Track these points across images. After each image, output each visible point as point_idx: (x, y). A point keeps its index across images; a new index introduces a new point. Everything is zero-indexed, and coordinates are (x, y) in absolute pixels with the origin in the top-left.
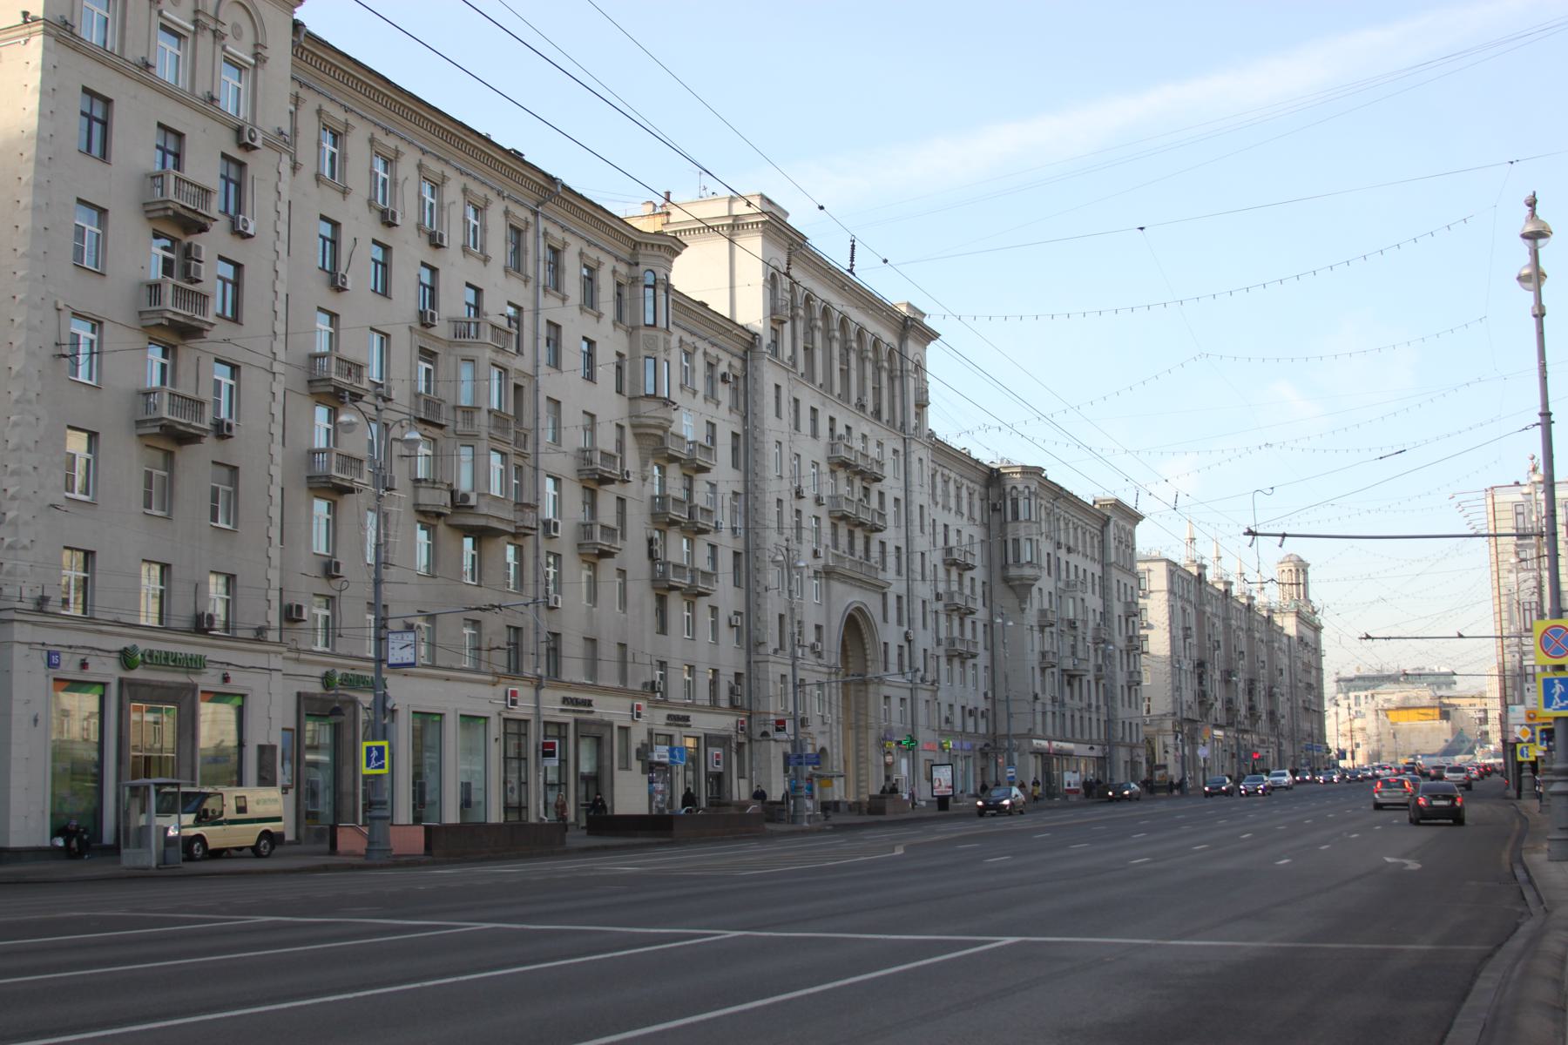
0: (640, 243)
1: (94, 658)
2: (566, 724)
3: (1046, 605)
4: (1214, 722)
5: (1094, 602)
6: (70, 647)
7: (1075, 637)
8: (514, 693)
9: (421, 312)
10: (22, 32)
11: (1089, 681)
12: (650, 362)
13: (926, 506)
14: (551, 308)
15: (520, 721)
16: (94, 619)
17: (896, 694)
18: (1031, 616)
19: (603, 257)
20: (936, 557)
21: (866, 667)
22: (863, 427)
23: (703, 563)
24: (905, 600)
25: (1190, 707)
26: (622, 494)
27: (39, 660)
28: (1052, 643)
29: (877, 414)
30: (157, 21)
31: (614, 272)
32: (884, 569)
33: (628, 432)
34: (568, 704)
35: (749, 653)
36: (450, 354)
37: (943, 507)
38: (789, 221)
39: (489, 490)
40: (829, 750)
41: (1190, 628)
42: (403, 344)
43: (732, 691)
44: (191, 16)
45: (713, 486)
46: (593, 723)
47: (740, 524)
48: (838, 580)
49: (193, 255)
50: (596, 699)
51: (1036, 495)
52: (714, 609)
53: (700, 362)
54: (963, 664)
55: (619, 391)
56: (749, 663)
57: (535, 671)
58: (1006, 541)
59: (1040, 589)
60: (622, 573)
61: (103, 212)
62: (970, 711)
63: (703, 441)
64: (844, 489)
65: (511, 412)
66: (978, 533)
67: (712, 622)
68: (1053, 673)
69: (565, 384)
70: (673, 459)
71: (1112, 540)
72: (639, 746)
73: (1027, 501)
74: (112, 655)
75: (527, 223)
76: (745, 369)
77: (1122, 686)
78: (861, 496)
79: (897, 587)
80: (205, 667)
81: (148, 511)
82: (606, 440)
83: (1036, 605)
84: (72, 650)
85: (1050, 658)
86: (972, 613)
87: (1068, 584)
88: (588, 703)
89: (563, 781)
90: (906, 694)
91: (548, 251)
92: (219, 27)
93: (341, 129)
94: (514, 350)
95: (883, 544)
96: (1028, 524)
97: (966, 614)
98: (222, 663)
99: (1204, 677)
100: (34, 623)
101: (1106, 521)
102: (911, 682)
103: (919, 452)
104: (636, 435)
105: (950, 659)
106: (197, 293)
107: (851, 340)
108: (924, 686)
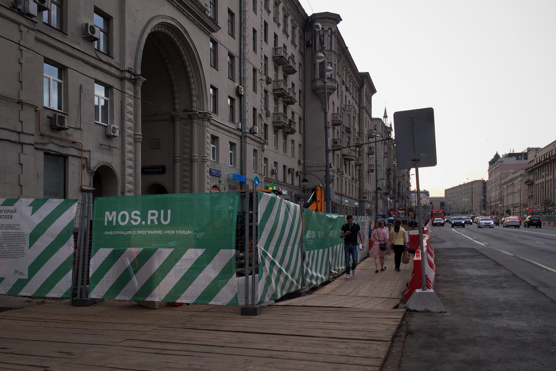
7: (349, 138)
21: (192, 102)
40: (117, 170)
62: (289, 170)
73: (329, 38)
96: (330, 53)
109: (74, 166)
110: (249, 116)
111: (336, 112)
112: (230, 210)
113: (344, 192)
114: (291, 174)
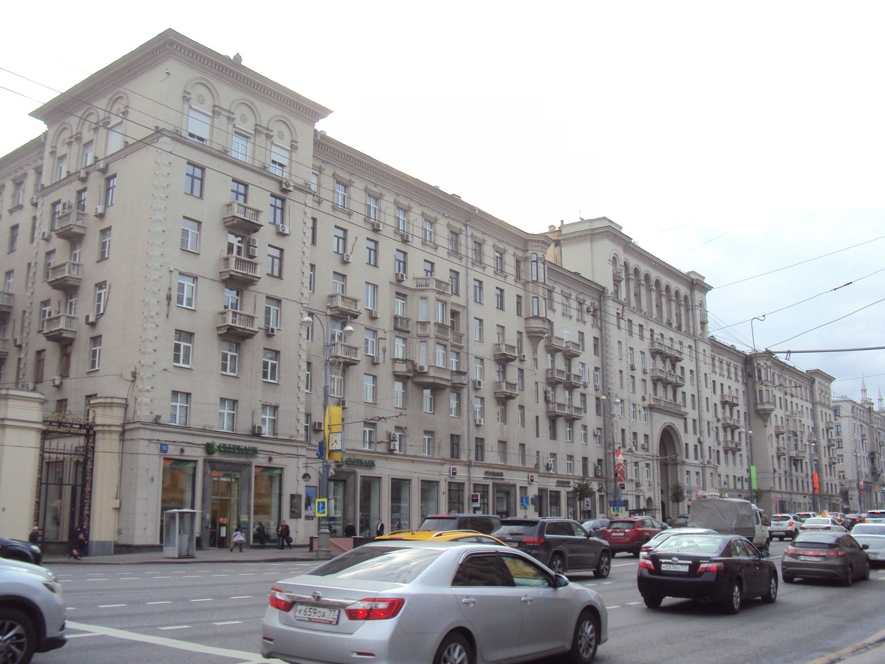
0: (528, 240)
2: (488, 486)
3: (779, 424)
5: (808, 422)
8: (454, 469)
9: (397, 274)
11: (806, 463)
12: (535, 300)
14: (476, 273)
17: (693, 471)
18: (771, 430)
22: (669, 334)
23: (577, 402)
25: (867, 476)
26: (521, 367)
27: (155, 449)
28: (784, 443)
29: (679, 328)
30: (231, 130)
32: (685, 406)
35: (605, 448)
37: (720, 375)
39: (435, 363)
40: (653, 498)
42: (386, 292)
43: (596, 469)
45: (583, 364)
46: (505, 485)
47: (599, 383)
48: (657, 412)
51: (771, 368)
52: (585, 427)
53: (574, 304)
54: (734, 454)
55: (519, 314)
56: (606, 454)
57: (468, 458)
60: (522, 407)
61: (199, 223)
62: (739, 479)
63: (577, 342)
65: (449, 324)
66: (741, 387)
68: (785, 458)
70: (558, 350)
71: (817, 390)
72: (533, 497)
75: (460, 230)
78: (670, 369)
79: (692, 414)
80: (257, 453)
81: (224, 373)
82: (511, 339)
83: (774, 423)
87: (792, 413)
88: (502, 474)
91: (474, 244)
92: (269, 133)
94: (450, 293)
95: (684, 393)
97: (735, 429)
98: (269, 451)
99: (875, 460)
100: (153, 430)
101: (813, 382)
103: (702, 346)
104: (529, 337)
105: (726, 452)
106: (253, 263)
108: (709, 466)
109: (642, 499)
110: (707, 454)
111: (779, 424)
113: (795, 490)
114: (740, 482)
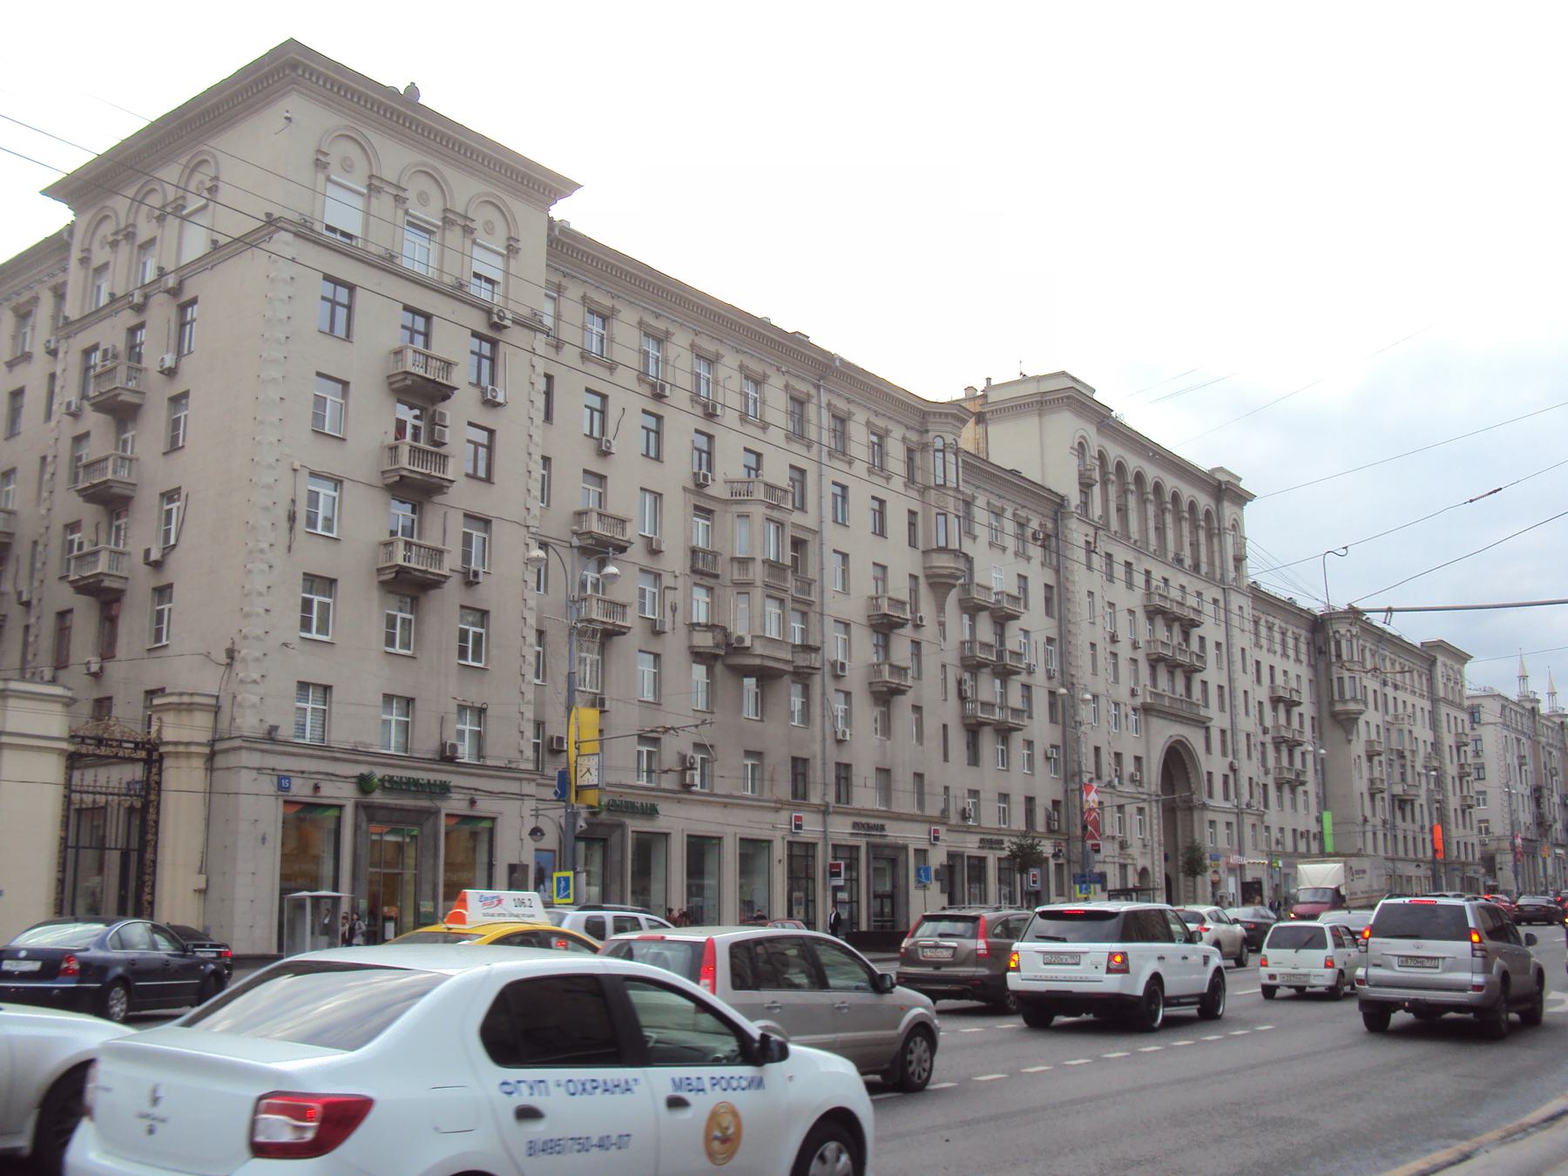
1: (328, 783)
2: (857, 848)
3: (1374, 736)
4: (1554, 842)
5: (1424, 733)
6: (303, 772)
8: (799, 818)
9: (695, 474)
10: (265, 232)
11: (1421, 805)
12: (942, 518)
13: (1247, 648)
14: (835, 471)
15: (807, 844)
16: (328, 748)
17: (1221, 819)
18: (1358, 748)
19: (891, 426)
20: (1263, 693)
22: (1177, 579)
23: (1015, 700)
24: (1229, 733)
25: (1528, 828)
26: (917, 637)
27: (268, 785)
29: (1196, 567)
31: (904, 439)
32: (1207, 706)
33: (922, 580)
34: (859, 829)
35: (1066, 781)
36: (726, 512)
37: (1269, 650)
38: (1096, 397)
39: (764, 631)
40: (1150, 869)
41: (1524, 757)
42: (677, 505)
43: (1049, 818)
44: (505, 244)
45: (1026, 632)
46: (887, 846)
47: (1055, 666)
48: (1158, 717)
49: (437, 421)
50: (888, 825)
52: (1029, 744)
53: (1010, 526)
55: (912, 543)
56: (1066, 791)
57: (823, 799)
58: (1331, 680)
59: (1367, 723)
60: (917, 709)
61: (345, 384)
62: (1302, 834)
63: (1015, 592)
64: (1162, 634)
66: (1305, 672)
67: (1029, 755)
69: (857, 538)
71: (1440, 678)
74: (349, 780)
76: (1056, 527)
77: (1456, 810)
79: (1219, 720)
82: (899, 587)
84: (305, 775)
85: (1378, 785)
86: (1300, 744)
88: (882, 828)
89: (855, 899)
90: (1233, 819)
92: (468, 223)
93: (607, 313)
95: (1204, 683)
98: (470, 789)
100: (263, 751)
102: (1237, 807)
103: (1236, 600)
105: (1279, 787)
107: (1166, 505)
108: (1249, 811)
109: (1130, 869)
111: (1374, 736)
112: (1199, 1010)
113: (1401, 853)
